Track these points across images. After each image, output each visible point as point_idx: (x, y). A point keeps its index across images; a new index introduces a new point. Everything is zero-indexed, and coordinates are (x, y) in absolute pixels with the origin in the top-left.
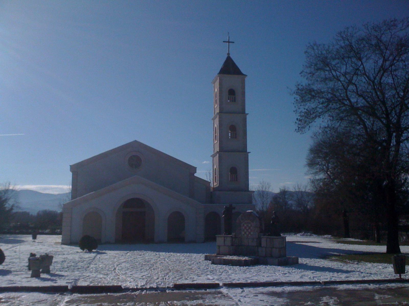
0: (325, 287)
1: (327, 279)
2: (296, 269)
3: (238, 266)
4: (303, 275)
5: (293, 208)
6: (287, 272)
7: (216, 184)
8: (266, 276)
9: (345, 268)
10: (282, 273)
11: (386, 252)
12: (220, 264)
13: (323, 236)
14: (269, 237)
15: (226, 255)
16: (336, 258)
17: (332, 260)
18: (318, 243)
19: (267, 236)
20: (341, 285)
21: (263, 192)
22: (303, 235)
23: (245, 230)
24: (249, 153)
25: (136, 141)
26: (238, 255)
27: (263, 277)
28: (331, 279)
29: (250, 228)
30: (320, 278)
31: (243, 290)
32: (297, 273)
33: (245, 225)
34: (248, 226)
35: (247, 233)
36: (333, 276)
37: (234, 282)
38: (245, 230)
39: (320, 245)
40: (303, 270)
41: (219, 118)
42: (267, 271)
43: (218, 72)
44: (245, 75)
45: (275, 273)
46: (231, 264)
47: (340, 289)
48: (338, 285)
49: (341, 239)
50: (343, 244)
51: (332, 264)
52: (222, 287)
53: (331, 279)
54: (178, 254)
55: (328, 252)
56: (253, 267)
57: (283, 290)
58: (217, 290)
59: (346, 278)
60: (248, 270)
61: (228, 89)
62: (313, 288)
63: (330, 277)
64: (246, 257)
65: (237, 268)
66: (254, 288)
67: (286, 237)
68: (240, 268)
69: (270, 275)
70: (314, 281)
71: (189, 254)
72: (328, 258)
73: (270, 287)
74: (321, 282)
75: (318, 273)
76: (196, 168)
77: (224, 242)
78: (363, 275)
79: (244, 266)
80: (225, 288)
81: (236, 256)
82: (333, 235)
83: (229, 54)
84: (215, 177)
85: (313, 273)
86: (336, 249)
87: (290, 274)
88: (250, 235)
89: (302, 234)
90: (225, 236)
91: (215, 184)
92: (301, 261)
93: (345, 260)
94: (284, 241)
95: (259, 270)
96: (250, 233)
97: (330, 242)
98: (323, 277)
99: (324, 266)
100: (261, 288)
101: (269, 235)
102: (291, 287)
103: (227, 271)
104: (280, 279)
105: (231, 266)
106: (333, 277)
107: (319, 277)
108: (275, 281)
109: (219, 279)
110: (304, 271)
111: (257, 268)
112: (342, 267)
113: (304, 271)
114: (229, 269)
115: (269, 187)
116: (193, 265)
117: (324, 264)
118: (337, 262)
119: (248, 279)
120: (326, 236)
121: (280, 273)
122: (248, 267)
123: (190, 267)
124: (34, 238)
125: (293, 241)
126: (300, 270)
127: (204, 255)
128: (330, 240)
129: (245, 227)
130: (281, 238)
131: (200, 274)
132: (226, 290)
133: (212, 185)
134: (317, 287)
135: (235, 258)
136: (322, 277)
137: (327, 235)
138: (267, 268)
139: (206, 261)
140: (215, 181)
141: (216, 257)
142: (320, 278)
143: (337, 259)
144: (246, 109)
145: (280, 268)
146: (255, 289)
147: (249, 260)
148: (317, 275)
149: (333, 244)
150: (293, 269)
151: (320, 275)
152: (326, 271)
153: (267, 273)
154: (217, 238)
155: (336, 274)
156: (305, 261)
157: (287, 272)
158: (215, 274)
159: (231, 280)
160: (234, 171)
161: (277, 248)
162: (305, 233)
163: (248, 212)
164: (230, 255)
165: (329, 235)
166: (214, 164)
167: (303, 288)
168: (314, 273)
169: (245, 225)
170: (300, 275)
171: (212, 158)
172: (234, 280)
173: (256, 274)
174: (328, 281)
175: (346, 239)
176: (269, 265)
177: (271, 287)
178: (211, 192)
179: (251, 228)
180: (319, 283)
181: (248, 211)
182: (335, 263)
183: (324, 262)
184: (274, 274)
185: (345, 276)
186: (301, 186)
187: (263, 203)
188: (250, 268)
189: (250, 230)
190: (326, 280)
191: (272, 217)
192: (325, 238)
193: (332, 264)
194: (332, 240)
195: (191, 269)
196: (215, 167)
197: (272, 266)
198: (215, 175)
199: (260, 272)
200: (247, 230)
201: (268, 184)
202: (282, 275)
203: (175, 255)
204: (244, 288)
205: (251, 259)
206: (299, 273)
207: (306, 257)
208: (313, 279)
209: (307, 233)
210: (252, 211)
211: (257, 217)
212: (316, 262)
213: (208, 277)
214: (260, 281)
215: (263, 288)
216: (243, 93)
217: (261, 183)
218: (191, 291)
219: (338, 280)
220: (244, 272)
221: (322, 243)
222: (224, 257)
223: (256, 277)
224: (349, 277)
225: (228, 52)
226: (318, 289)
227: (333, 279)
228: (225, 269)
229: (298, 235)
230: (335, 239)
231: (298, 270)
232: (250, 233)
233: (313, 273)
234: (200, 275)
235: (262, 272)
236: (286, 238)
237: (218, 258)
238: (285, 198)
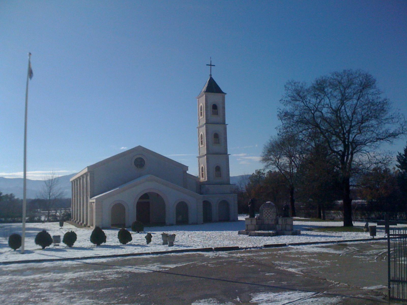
11: (144, 228)
14: (284, 218)
24: (229, 155)
25: (140, 147)
29: (269, 213)
33: (266, 211)
34: (268, 211)
35: (268, 216)
38: (266, 214)
41: (206, 127)
43: (204, 89)
44: (224, 93)
61: (212, 105)
76: (188, 167)
77: (251, 222)
78: (352, 238)
83: (211, 75)
84: (202, 174)
88: (269, 217)
96: (269, 216)
124: (61, 225)
129: (266, 213)
135: (263, 232)
144: (226, 120)
160: (218, 169)
169: (266, 211)
171: (197, 159)
180: (335, 242)
181: (267, 202)
189: (269, 214)
216: (224, 108)
225: (210, 74)
232: (269, 216)
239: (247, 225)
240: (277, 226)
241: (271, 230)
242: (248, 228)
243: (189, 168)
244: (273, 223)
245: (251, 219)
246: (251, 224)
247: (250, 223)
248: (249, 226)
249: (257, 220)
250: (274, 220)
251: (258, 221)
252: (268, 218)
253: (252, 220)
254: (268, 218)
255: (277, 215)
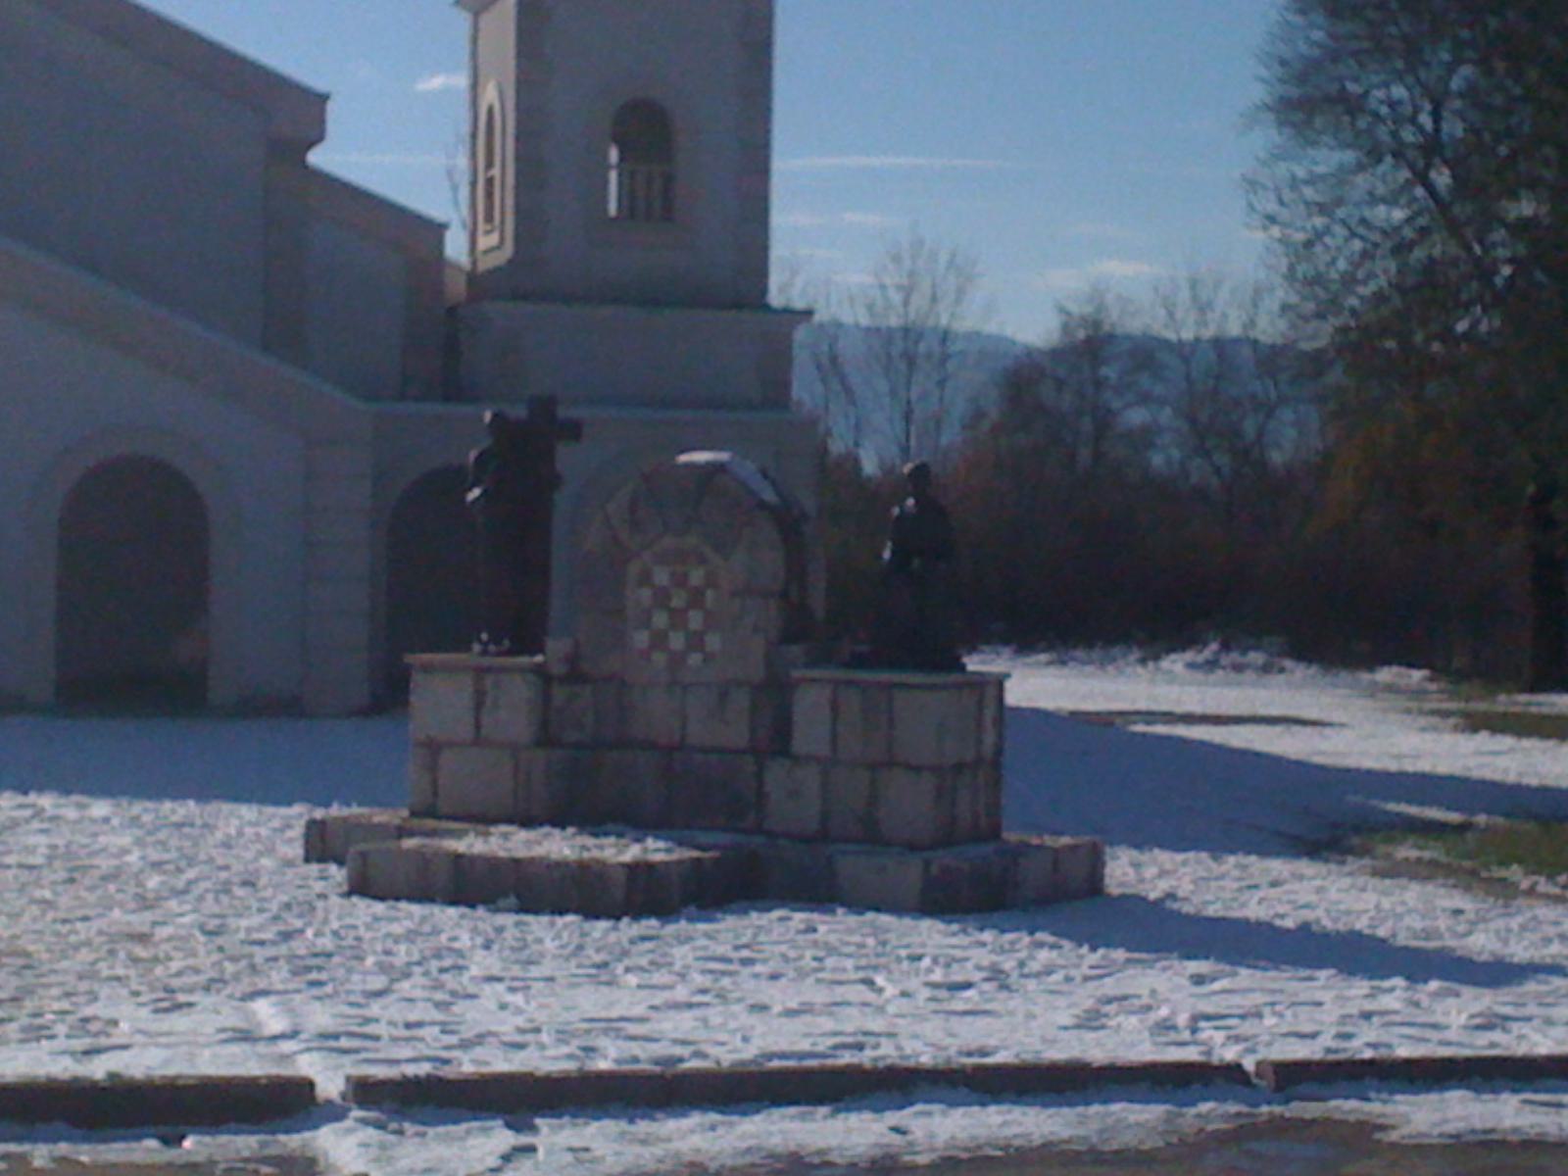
0: (1277, 1109)
1: (1314, 1036)
2: (1067, 944)
3: (570, 918)
4: (1109, 1001)
5: (1157, 460)
6: (979, 968)
7: (494, 239)
8: (777, 1009)
9: (1481, 943)
10: (937, 976)
12: (422, 894)
13: (1365, 677)
15: (483, 819)
16: (1427, 855)
17: (1393, 871)
18: (1309, 730)
19: (847, 665)
20: (1421, 1098)
21: (910, 333)
22: (1211, 665)
23: (660, 620)
26: (592, 819)
27: (753, 1020)
28: (1347, 1036)
30: (1247, 1028)
31: (524, 1139)
32: (1068, 979)
33: (662, 577)
34: (681, 581)
35: (677, 641)
36: (1369, 1006)
37: (467, 1065)
38: (660, 620)
39: (1324, 746)
40: (1120, 954)
42: (808, 962)
45: (869, 983)
46: (512, 900)
47: (1405, 1131)
48: (1392, 1092)
49: (1502, 698)
50: (1507, 741)
51: (1386, 904)
52: (333, 1113)
53: (1347, 1036)
54: (100, 808)
55: (1374, 802)
56: (702, 927)
57: (897, 1139)
58: (282, 1138)
59: (1478, 1027)
60: (648, 945)
62: (1169, 1119)
63: (1345, 1018)
64: (650, 843)
65: (551, 933)
66: (631, 1121)
67: (1008, 676)
68: (584, 934)
69: (820, 996)
70: (1191, 1054)
71: (191, 803)
72: (1364, 852)
73: (777, 1113)
74: (1249, 1064)
75: (1246, 985)
76: (323, 99)
77: (479, 706)
79: (618, 918)
80: (365, 1122)
81: (570, 830)
82: (1439, 669)
84: (490, 182)
85: (1199, 980)
86: (1451, 779)
87: (1004, 987)
88: (695, 659)
89: (1200, 658)
90: (487, 661)
91: (485, 242)
92: (1131, 871)
93: (1502, 873)
94: (989, 713)
95: (745, 953)
96: (696, 642)
97: (1408, 719)
98: (1280, 1015)
99: (1308, 915)
100: (695, 1119)
101: (858, 662)
102: (976, 1109)
103: (447, 962)
104: (891, 1035)
105: (508, 910)
106: (1367, 1016)
107: (1243, 1017)
108: (846, 1058)
109: (336, 1036)
110: (1129, 961)
111: (730, 930)
112: (1461, 928)
113: (1129, 961)
114: (479, 940)
115: (960, 293)
116: (173, 904)
117: (1313, 898)
118: (1430, 888)
119: (606, 1032)
120: (1385, 675)
121: (913, 984)
122: (653, 922)
123: (140, 921)
125: (1121, 714)
126: (1101, 951)
127: (299, 814)
128: (1414, 705)
129: (662, 597)
130: (959, 686)
131: (191, 990)
132: (365, 1145)
133: (455, 247)
134: (1210, 1112)
135: (559, 845)
136: (1270, 1021)
137: (1395, 669)
138: (822, 929)
139: (314, 868)
140: (489, 218)
141: (402, 832)
142: (1247, 1028)
143: (1433, 863)
145: (931, 934)
146: (643, 1127)
147: (666, 864)
148: (1236, 1000)
149: (1429, 737)
150: (1041, 945)
151: (1259, 998)
152: (1321, 967)
153: (802, 974)
154: (418, 678)
155: (1394, 995)
156: (1163, 873)
157: (979, 968)
158: (329, 989)
159: (453, 1040)
161: (918, 769)
162: (1226, 647)
163: (691, 466)
164: (527, 822)
165: (1411, 665)
166: (482, 72)
167: (1083, 1120)
168: (1214, 979)
170: (1085, 997)
172: (480, 1039)
173: (704, 991)
174: (1318, 1056)
175: (1541, 698)
176: (843, 905)
177: (792, 1110)
178: (452, 311)
179: (710, 594)
180: (1232, 1075)
181: (684, 458)
182: (1413, 893)
183: (1318, 882)
184: (861, 993)
185: (1476, 1008)
186: (1218, 285)
187: (908, 417)
188: (671, 929)
189: (695, 620)
190: (1300, 1051)
191: (896, 511)
192: (1374, 691)
193: (1386, 904)
194: (1428, 706)
195: (143, 938)
196: (490, 95)
197: (870, 916)
198: (489, 165)
199: (746, 971)
200: (678, 618)
201: (951, 263)
202: (926, 993)
203: (71, 813)
204: (538, 1121)
205: (695, 854)
206: (1086, 979)
207: (1179, 843)
208: (1186, 1035)
209: (1244, 651)
210: (723, 456)
211: (762, 505)
212: (1256, 886)
213: (250, 1016)
214: (714, 1051)
215: (713, 1117)
217: (897, 259)
218: (26, 1147)
219: (1404, 1051)
220: (605, 965)
221: (1342, 725)
222: (459, 835)
223: (688, 1015)
224: (1506, 1018)
226: (1210, 1128)
227: (1361, 1047)
228: (443, 938)
229: (1175, 663)
230: (1453, 696)
231: (1085, 949)
232: (696, 642)
233: (1199, 980)
234: (182, 998)
235: (759, 968)
236: (1008, 685)
237: (409, 843)
238: (1099, 384)
239: (433, 748)
240: (776, 775)
241: (634, 822)
242: (435, 794)
243: (330, 106)
244: (736, 733)
245: (481, 671)
246: (478, 741)
247: (465, 731)
248: (447, 757)
249: (546, 697)
250: (741, 699)
251: (559, 694)
252: (677, 660)
253: (489, 681)
254: (677, 660)
255: (789, 636)
